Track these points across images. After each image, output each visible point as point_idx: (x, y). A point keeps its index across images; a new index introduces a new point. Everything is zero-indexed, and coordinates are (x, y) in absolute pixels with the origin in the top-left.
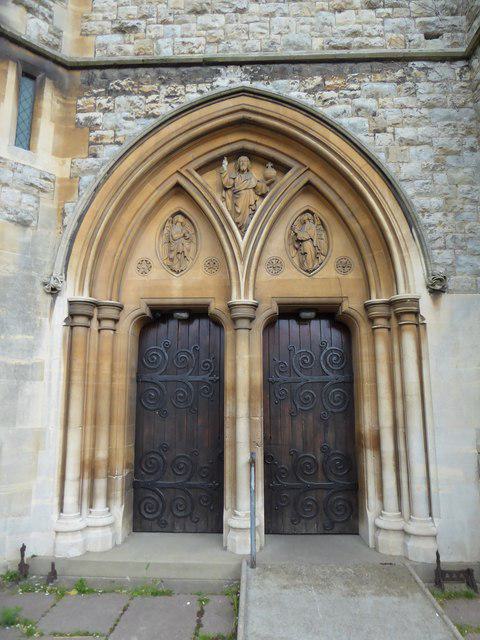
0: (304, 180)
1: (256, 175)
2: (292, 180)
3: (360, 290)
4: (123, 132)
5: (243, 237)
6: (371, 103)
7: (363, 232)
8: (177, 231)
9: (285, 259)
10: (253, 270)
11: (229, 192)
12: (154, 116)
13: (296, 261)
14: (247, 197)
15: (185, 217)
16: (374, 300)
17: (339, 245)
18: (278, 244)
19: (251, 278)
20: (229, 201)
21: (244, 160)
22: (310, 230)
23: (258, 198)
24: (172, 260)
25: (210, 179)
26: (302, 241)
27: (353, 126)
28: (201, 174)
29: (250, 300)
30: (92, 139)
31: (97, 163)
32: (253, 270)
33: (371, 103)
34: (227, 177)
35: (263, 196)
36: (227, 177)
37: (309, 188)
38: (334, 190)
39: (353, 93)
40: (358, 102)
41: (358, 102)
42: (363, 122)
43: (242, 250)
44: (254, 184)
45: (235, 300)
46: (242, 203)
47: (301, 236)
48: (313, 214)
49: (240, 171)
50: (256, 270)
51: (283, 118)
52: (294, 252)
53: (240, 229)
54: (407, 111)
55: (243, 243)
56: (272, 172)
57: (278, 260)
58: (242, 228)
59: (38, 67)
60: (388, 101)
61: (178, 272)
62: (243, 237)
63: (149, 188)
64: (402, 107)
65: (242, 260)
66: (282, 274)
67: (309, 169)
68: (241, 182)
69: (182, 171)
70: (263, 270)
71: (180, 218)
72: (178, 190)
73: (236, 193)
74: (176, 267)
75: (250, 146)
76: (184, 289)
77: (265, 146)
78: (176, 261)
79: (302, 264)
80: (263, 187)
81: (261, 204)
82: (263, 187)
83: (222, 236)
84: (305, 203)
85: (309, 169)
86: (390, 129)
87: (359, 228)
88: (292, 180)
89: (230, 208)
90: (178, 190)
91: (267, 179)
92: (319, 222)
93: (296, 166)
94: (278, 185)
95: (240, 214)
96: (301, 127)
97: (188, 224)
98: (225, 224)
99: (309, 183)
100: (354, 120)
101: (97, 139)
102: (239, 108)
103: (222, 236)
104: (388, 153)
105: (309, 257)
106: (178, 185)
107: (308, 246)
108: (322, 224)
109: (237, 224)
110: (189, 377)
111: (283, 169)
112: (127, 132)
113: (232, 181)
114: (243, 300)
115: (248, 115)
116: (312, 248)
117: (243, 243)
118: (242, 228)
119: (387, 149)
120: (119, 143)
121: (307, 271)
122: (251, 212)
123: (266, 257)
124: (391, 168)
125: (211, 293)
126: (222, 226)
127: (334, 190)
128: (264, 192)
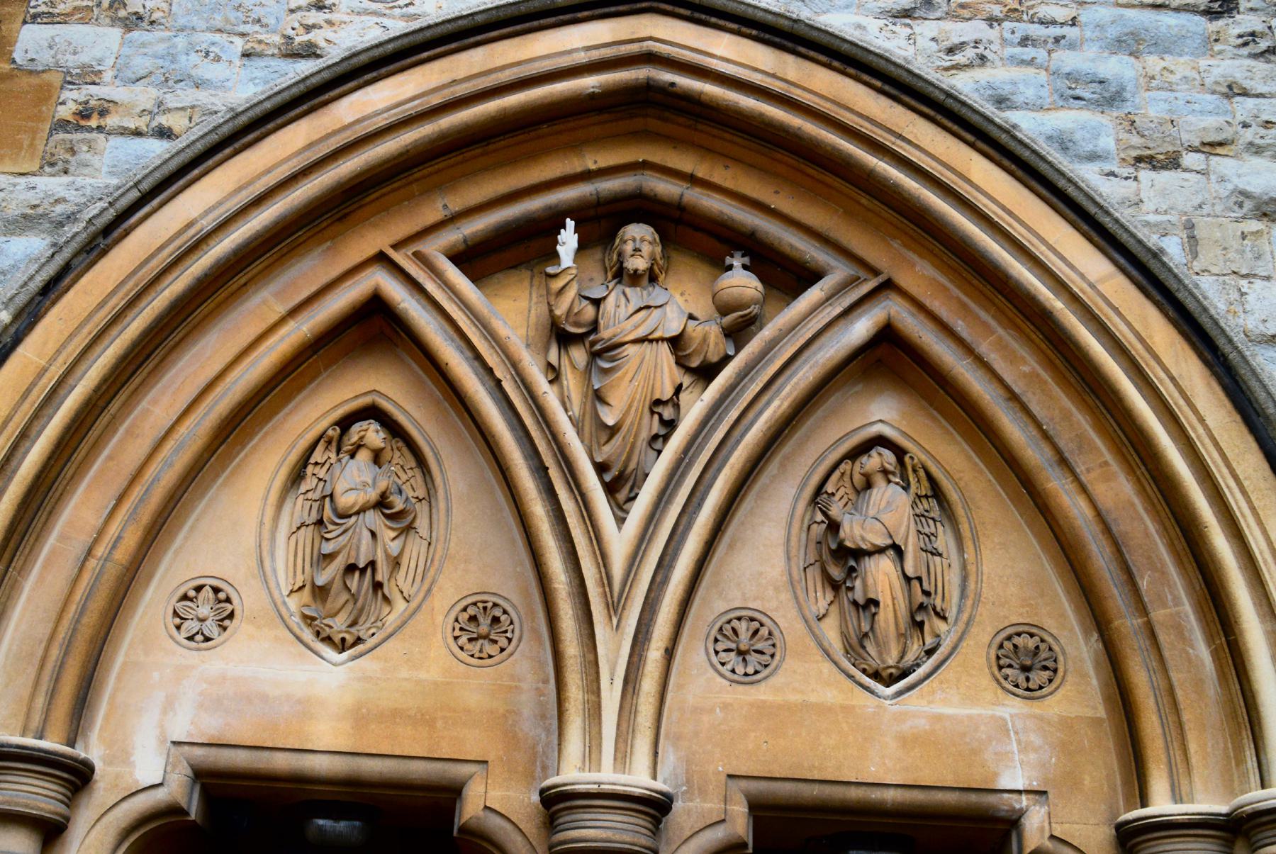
0: (861, 328)
1: (681, 303)
2: (822, 326)
3: (1100, 767)
4: (187, 96)
5: (621, 521)
6: (1117, 67)
7: (1107, 529)
8: (354, 480)
9: (787, 619)
10: (654, 654)
11: (579, 355)
12: (310, 51)
13: (831, 631)
14: (656, 371)
15: (393, 428)
16: (1162, 805)
17: (1003, 576)
18: (764, 564)
19: (649, 684)
20: (571, 381)
21: (639, 241)
22: (886, 512)
23: (686, 380)
24: (321, 593)
25: (512, 312)
26: (859, 554)
27: (1063, 142)
28: (476, 278)
29: (638, 779)
30: (65, 112)
31: (71, 195)
32: (654, 654)
33: (1117, 67)
34: (571, 293)
35: (706, 373)
36: (571, 293)
37: (888, 358)
38: (989, 365)
39: (1056, 31)
40: (1067, 60)
41: (1067, 60)
42: (1099, 129)
43: (616, 594)
44: (673, 329)
45: (572, 772)
46: (625, 397)
47: (855, 531)
48: (900, 452)
49: (621, 275)
50: (670, 653)
51: (797, 94)
52: (822, 600)
53: (611, 489)
54: (1244, 107)
55: (619, 541)
56: (741, 282)
57: (757, 623)
58: (620, 485)
59: (3, 273)
60: (1181, 66)
61: (342, 646)
62: (621, 521)
63: (263, 303)
64: (1234, 91)
65: (615, 607)
66: (777, 680)
67: (888, 286)
68: (621, 312)
69: (398, 257)
70: (694, 653)
71: (373, 434)
72: (373, 329)
73: (605, 355)
74: (338, 625)
75: (665, 188)
76: (360, 716)
77: (720, 189)
78: (343, 603)
79: (856, 646)
80: (709, 336)
81: (695, 407)
82: (709, 336)
83: (538, 509)
84: (882, 412)
85: (888, 286)
86: (1189, 159)
87: (1088, 512)
88: (822, 326)
89: (576, 410)
90: (381, 258)
91: (724, 310)
92: (925, 489)
93: (839, 270)
94: (767, 332)
95: (613, 431)
96: (866, 128)
97: (399, 457)
98: (552, 464)
99: (887, 335)
100: (1067, 119)
101: (85, 114)
102: (634, 48)
103: (538, 509)
104: (1193, 241)
105: (885, 616)
106: (376, 305)
107: (881, 575)
108: (936, 492)
109: (601, 468)
110: (534, 296)
111: (786, 276)
112: (203, 97)
113: (590, 311)
114: (608, 776)
115: (667, 76)
116: (898, 583)
117: (619, 541)
118: (620, 485)
119: (1190, 226)
120: (164, 133)
121: (876, 676)
122: (656, 428)
123: (713, 605)
124: (1213, 294)
125: (472, 743)
126: (541, 471)
127: (989, 365)
128: (714, 358)
